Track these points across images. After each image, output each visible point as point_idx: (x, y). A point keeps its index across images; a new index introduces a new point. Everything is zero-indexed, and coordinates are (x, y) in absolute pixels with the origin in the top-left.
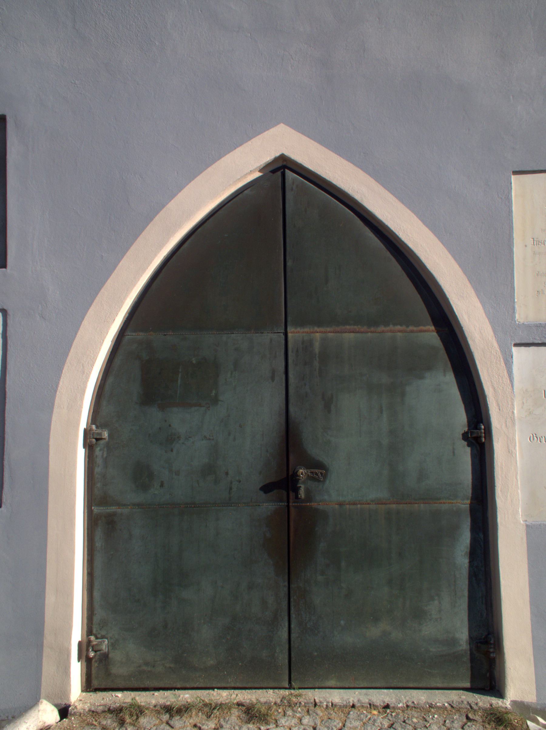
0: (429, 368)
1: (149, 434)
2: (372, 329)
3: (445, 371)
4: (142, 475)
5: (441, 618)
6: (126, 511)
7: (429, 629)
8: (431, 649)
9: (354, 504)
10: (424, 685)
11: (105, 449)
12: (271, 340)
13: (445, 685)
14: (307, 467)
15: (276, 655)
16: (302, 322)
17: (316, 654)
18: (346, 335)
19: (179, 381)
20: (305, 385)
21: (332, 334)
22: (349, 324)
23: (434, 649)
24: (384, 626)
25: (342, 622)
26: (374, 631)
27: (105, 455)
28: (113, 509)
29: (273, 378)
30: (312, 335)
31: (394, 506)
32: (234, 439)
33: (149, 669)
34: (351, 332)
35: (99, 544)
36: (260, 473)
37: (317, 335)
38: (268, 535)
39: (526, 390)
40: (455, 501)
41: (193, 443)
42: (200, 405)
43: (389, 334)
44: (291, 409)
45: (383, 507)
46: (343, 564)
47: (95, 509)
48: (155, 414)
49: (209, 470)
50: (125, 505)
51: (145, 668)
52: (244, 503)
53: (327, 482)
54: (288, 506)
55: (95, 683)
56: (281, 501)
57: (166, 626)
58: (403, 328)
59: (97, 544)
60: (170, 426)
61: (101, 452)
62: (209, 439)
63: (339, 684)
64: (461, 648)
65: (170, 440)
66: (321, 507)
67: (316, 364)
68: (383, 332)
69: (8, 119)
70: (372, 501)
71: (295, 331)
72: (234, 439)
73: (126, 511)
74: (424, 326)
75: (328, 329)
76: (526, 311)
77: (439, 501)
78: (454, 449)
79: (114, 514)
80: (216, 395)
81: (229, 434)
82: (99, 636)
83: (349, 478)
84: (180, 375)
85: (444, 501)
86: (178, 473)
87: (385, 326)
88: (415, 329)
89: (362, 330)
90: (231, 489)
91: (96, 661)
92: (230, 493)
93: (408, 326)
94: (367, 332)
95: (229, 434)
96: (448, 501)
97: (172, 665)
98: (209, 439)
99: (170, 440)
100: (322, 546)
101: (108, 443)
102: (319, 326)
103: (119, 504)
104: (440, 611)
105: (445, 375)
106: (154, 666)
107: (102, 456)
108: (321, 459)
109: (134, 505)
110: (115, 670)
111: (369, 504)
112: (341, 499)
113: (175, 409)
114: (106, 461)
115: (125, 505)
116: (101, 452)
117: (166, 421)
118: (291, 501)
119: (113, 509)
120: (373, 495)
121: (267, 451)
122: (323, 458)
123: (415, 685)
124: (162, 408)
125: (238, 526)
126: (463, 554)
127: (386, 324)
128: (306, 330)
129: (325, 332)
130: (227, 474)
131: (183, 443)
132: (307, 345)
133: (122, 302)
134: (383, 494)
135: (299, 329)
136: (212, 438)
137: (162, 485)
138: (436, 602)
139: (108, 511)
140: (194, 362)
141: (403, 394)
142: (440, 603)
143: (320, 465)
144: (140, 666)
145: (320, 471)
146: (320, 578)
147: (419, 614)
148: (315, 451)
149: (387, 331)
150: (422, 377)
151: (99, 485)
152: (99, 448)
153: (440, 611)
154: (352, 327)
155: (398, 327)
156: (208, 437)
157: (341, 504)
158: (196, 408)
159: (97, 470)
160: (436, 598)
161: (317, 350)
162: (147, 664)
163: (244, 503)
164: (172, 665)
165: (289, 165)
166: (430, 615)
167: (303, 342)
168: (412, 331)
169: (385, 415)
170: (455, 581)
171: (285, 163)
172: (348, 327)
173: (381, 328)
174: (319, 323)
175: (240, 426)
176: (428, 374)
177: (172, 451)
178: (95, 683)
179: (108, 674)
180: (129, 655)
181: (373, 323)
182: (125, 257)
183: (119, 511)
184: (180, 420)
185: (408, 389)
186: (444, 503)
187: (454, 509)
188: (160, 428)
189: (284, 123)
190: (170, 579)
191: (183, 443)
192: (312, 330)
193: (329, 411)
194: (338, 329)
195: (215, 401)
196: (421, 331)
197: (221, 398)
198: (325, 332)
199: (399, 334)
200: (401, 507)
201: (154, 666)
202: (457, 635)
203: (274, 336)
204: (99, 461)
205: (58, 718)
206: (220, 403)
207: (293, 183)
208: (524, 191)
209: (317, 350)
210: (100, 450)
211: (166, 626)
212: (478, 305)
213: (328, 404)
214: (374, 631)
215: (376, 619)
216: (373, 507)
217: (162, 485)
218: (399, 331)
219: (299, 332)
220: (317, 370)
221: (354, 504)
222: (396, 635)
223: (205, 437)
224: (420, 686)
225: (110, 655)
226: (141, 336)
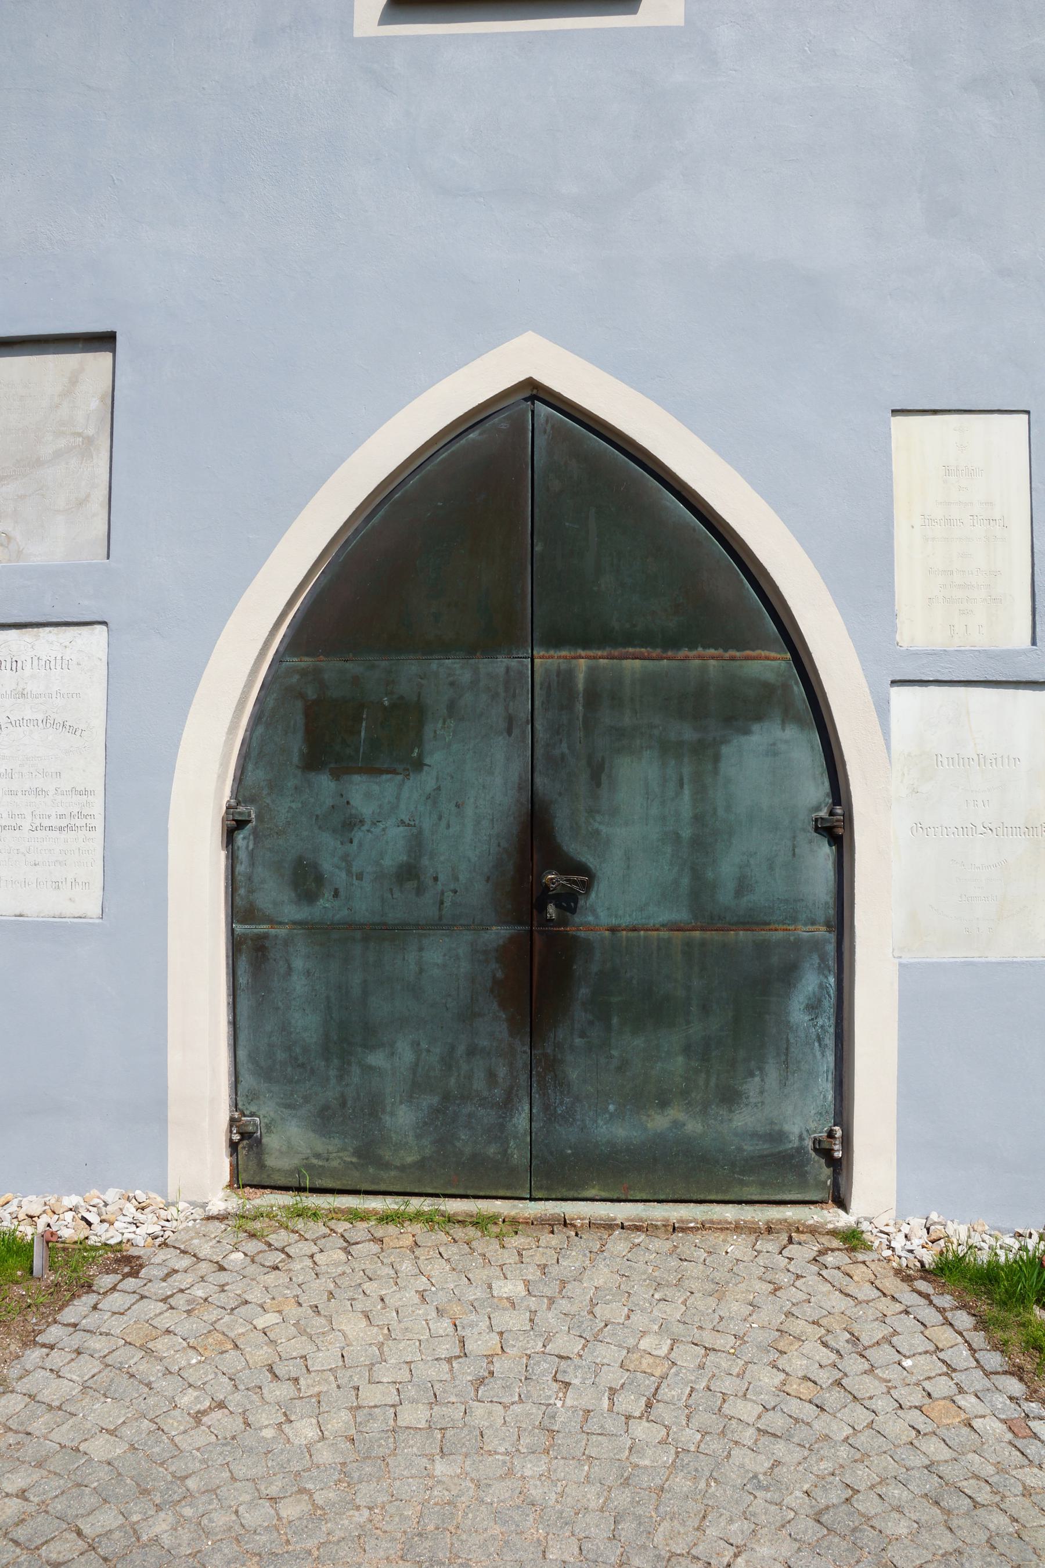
0: (759, 718)
1: (317, 816)
2: (670, 653)
3: (783, 722)
4: (306, 880)
5: (763, 1103)
6: (282, 932)
7: (744, 1119)
8: (745, 1147)
9: (634, 929)
10: (733, 1198)
11: (251, 837)
12: (508, 669)
13: (765, 1198)
14: (561, 872)
15: (509, 1151)
16: (556, 640)
17: (569, 1152)
18: (627, 663)
19: (363, 734)
20: (561, 741)
21: (606, 661)
22: (634, 646)
23: (748, 1147)
24: (675, 1113)
25: (611, 1108)
26: (659, 1122)
27: (251, 847)
28: (263, 928)
29: (509, 731)
30: (574, 661)
31: (697, 934)
32: (448, 826)
33: (320, 1163)
34: (636, 658)
35: (242, 980)
36: (488, 879)
37: (582, 665)
38: (499, 975)
39: (909, 755)
40: (792, 927)
41: (384, 830)
42: (393, 772)
43: (697, 662)
44: (538, 780)
45: (680, 934)
46: (615, 1021)
47: (239, 928)
48: (324, 782)
49: (409, 874)
50: (280, 923)
51: (315, 1161)
52: (461, 925)
53: (593, 895)
54: (531, 931)
55: (243, 1177)
56: (520, 923)
57: (343, 1104)
58: (720, 652)
59: (241, 981)
60: (348, 803)
61: (245, 842)
62: (409, 825)
63: (604, 1195)
64: (790, 1146)
65: (349, 824)
66: (582, 934)
67: (579, 708)
68: (687, 658)
69: (118, 335)
70: (663, 925)
71: (546, 654)
72: (448, 826)
73: (282, 932)
74: (753, 650)
75: (599, 653)
76: (921, 626)
77: (768, 927)
78: (794, 847)
79: (265, 936)
80: (420, 755)
81: (440, 818)
82: (247, 1113)
83: (627, 890)
84: (364, 724)
85: (776, 926)
86: (360, 877)
87: (691, 649)
88: (738, 654)
89: (654, 655)
90: (442, 903)
91: (244, 1148)
92: (440, 909)
93: (726, 650)
94: (662, 659)
95: (440, 818)
96: (781, 926)
97: (354, 1160)
98: (409, 825)
99: (349, 824)
100: (583, 992)
101: (255, 828)
102: (584, 649)
103: (272, 922)
104: (762, 1092)
105: (784, 730)
106: (327, 1160)
107: (247, 847)
108: (584, 860)
109: (294, 923)
110: (271, 1162)
111: (657, 930)
112: (614, 921)
113: (356, 778)
114: (252, 855)
115: (280, 923)
116: (245, 842)
117: (342, 795)
118: (535, 923)
119: (263, 928)
120: (665, 916)
121: (499, 846)
122: (589, 859)
123: (719, 1197)
124: (337, 775)
125: (447, 962)
126: (802, 1007)
127: (692, 646)
128: (564, 653)
129: (595, 658)
130: (436, 879)
131: (368, 831)
132: (566, 678)
134: (682, 915)
135: (552, 653)
136: (412, 823)
137: (336, 894)
138: (757, 1079)
139: (255, 931)
140: (386, 703)
141: (717, 758)
142: (762, 1080)
143: (582, 869)
144: (307, 1159)
145: (584, 877)
146: (578, 1041)
147: (730, 1097)
148: (574, 848)
149: (694, 658)
150: (747, 732)
151: (242, 891)
152: (567, 838)
153: (762, 1092)
154: (638, 650)
155: (712, 651)
156: (407, 821)
157: (613, 930)
158: (389, 776)
159: (240, 868)
160: (757, 1073)
161: (581, 686)
162: (318, 1156)
163: (461, 925)
164: (354, 1160)
165: (541, 395)
166: (747, 1098)
167: (559, 673)
168: (733, 659)
169: (687, 791)
170: (787, 1049)
171: (535, 392)
172: (631, 650)
173: (684, 652)
174: (585, 643)
175: (457, 806)
176: (756, 727)
177: (351, 842)
178: (243, 1177)
179: (261, 1166)
180: (290, 1141)
181: (671, 642)
182: (283, 540)
183: (273, 931)
184: (364, 794)
185: (725, 750)
186: (776, 930)
187: (792, 938)
188: (333, 807)
189: (534, 331)
190: (348, 1036)
191: (368, 831)
192: (572, 654)
193: (598, 784)
194: (616, 652)
195: (418, 765)
196: (747, 658)
197: (427, 761)
198: (595, 658)
199: (712, 662)
200: (708, 934)
201: (327, 1160)
202: (786, 1128)
203: (514, 663)
204: (242, 855)
206: (426, 768)
207: (547, 421)
209: (581, 686)
210: (244, 838)
211: (343, 1104)
212: (838, 618)
213: (597, 772)
214: (659, 1122)
215: (664, 1104)
216: (664, 934)
217: (336, 894)
218: (713, 658)
219: (552, 657)
220: (581, 719)
221: (634, 929)
222: (694, 1126)
223: (402, 822)
224: (727, 1198)
225: (264, 1140)
226: (307, 662)
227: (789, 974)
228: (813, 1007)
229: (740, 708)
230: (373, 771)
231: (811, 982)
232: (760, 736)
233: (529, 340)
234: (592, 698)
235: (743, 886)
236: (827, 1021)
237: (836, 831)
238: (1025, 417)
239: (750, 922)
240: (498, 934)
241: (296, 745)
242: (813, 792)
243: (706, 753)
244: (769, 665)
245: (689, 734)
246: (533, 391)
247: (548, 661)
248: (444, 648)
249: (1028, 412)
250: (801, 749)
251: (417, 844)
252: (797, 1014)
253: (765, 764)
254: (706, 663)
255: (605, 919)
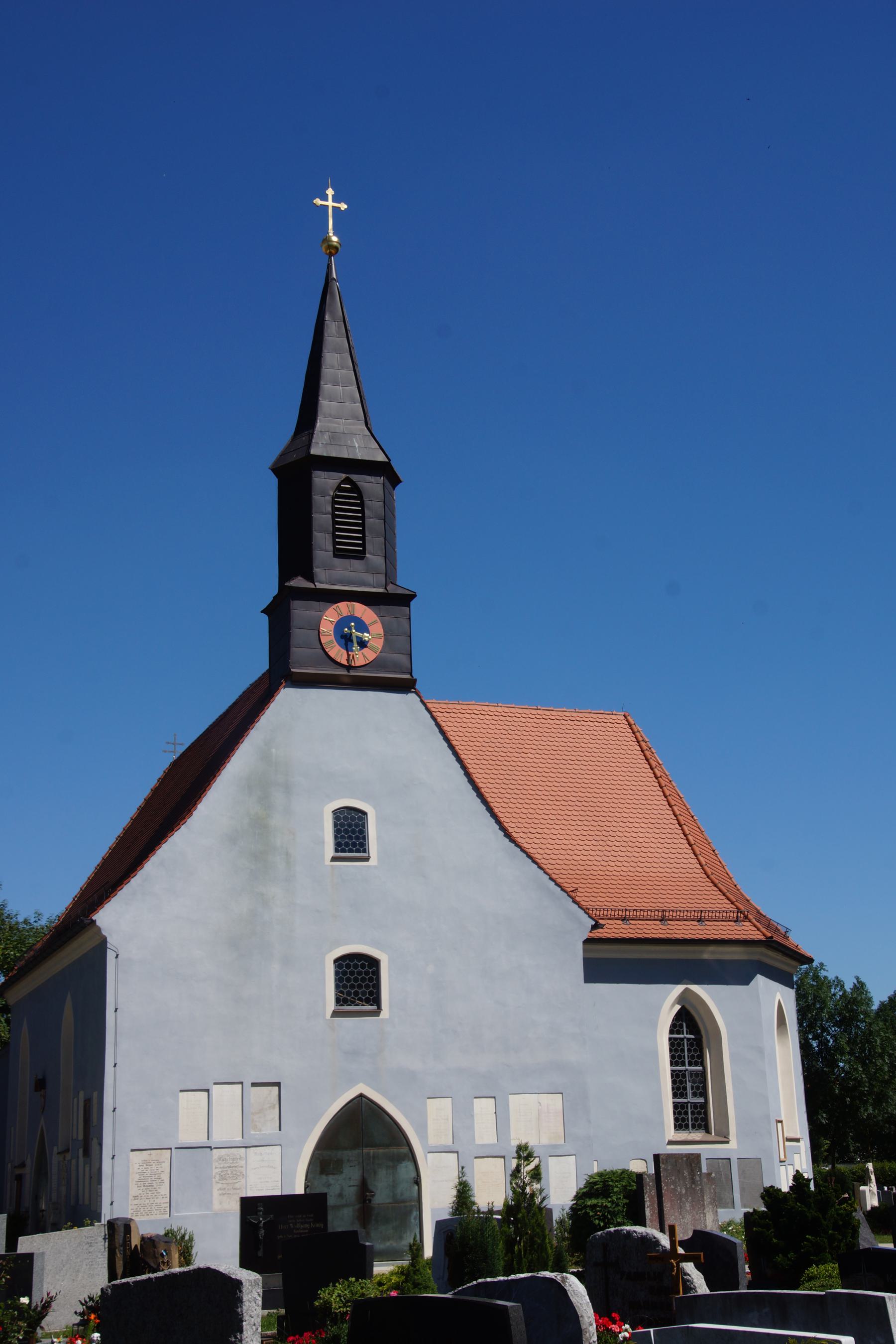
16: (367, 1147)
24: (391, 1242)
26: (388, 1244)
37: (372, 1151)
48: (324, 1177)
49: (340, 1195)
76: (432, 1141)
83: (381, 1197)
99: (329, 1185)
120: (388, 1201)
122: (374, 1190)
132: (368, 1154)
133: (738, 1125)
148: (371, 1188)
181: (388, 1146)
184: (331, 1179)
195: (342, 1172)
205: (412, 697)
208: (3, 1253)
213: (375, 1173)
222: (395, 1245)
227: (410, 1212)
228: (415, 1218)
229: (400, 1159)
230: (333, 1174)
231: (415, 1213)
232: (404, 1164)
233: (374, 811)
234: (374, 1157)
235: (402, 1194)
236: (418, 1221)
237: (417, 1182)
238: (277, 1088)
239: (403, 1201)
240: (357, 1207)
241: (318, 1169)
242: (414, 1174)
243: (394, 1168)
244: (405, 1150)
245: (391, 1164)
246: (335, 812)
247: (366, 1150)
248: (346, 1149)
249: (242, 1083)
250: (411, 1166)
251: (342, 1189)
252: (413, 1221)
253: (405, 1171)
254: (394, 1150)
255: (377, 1202)
